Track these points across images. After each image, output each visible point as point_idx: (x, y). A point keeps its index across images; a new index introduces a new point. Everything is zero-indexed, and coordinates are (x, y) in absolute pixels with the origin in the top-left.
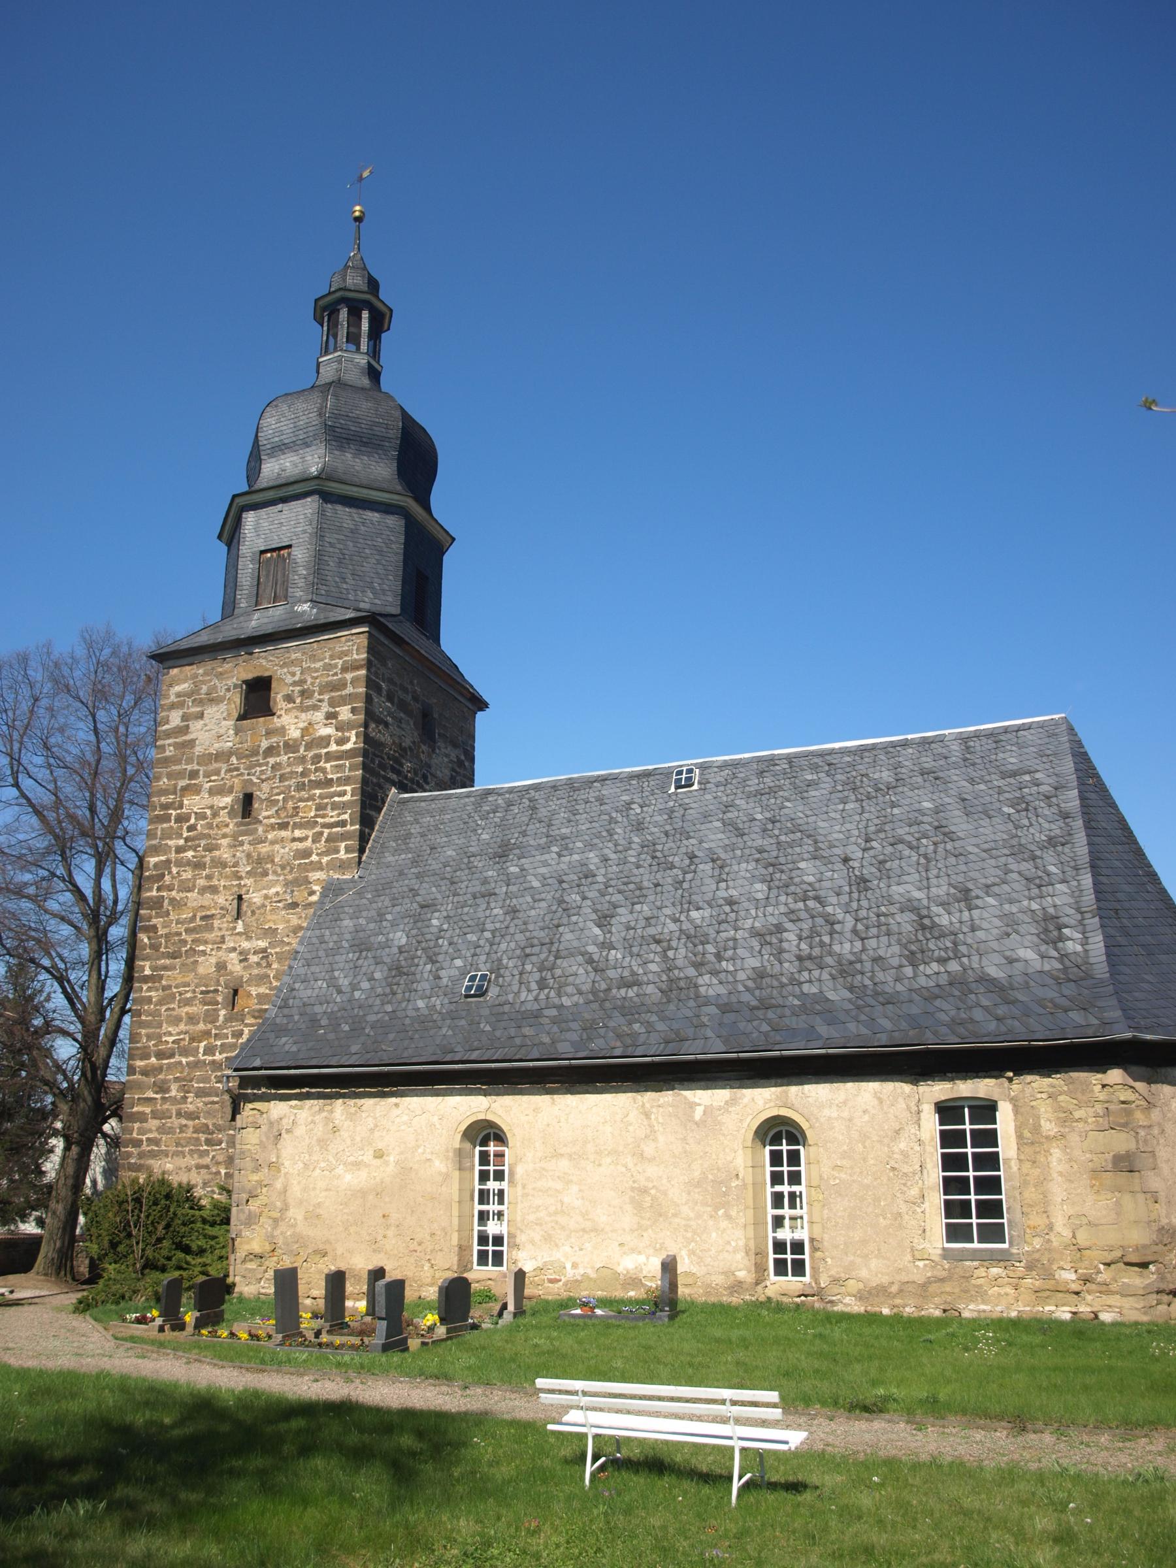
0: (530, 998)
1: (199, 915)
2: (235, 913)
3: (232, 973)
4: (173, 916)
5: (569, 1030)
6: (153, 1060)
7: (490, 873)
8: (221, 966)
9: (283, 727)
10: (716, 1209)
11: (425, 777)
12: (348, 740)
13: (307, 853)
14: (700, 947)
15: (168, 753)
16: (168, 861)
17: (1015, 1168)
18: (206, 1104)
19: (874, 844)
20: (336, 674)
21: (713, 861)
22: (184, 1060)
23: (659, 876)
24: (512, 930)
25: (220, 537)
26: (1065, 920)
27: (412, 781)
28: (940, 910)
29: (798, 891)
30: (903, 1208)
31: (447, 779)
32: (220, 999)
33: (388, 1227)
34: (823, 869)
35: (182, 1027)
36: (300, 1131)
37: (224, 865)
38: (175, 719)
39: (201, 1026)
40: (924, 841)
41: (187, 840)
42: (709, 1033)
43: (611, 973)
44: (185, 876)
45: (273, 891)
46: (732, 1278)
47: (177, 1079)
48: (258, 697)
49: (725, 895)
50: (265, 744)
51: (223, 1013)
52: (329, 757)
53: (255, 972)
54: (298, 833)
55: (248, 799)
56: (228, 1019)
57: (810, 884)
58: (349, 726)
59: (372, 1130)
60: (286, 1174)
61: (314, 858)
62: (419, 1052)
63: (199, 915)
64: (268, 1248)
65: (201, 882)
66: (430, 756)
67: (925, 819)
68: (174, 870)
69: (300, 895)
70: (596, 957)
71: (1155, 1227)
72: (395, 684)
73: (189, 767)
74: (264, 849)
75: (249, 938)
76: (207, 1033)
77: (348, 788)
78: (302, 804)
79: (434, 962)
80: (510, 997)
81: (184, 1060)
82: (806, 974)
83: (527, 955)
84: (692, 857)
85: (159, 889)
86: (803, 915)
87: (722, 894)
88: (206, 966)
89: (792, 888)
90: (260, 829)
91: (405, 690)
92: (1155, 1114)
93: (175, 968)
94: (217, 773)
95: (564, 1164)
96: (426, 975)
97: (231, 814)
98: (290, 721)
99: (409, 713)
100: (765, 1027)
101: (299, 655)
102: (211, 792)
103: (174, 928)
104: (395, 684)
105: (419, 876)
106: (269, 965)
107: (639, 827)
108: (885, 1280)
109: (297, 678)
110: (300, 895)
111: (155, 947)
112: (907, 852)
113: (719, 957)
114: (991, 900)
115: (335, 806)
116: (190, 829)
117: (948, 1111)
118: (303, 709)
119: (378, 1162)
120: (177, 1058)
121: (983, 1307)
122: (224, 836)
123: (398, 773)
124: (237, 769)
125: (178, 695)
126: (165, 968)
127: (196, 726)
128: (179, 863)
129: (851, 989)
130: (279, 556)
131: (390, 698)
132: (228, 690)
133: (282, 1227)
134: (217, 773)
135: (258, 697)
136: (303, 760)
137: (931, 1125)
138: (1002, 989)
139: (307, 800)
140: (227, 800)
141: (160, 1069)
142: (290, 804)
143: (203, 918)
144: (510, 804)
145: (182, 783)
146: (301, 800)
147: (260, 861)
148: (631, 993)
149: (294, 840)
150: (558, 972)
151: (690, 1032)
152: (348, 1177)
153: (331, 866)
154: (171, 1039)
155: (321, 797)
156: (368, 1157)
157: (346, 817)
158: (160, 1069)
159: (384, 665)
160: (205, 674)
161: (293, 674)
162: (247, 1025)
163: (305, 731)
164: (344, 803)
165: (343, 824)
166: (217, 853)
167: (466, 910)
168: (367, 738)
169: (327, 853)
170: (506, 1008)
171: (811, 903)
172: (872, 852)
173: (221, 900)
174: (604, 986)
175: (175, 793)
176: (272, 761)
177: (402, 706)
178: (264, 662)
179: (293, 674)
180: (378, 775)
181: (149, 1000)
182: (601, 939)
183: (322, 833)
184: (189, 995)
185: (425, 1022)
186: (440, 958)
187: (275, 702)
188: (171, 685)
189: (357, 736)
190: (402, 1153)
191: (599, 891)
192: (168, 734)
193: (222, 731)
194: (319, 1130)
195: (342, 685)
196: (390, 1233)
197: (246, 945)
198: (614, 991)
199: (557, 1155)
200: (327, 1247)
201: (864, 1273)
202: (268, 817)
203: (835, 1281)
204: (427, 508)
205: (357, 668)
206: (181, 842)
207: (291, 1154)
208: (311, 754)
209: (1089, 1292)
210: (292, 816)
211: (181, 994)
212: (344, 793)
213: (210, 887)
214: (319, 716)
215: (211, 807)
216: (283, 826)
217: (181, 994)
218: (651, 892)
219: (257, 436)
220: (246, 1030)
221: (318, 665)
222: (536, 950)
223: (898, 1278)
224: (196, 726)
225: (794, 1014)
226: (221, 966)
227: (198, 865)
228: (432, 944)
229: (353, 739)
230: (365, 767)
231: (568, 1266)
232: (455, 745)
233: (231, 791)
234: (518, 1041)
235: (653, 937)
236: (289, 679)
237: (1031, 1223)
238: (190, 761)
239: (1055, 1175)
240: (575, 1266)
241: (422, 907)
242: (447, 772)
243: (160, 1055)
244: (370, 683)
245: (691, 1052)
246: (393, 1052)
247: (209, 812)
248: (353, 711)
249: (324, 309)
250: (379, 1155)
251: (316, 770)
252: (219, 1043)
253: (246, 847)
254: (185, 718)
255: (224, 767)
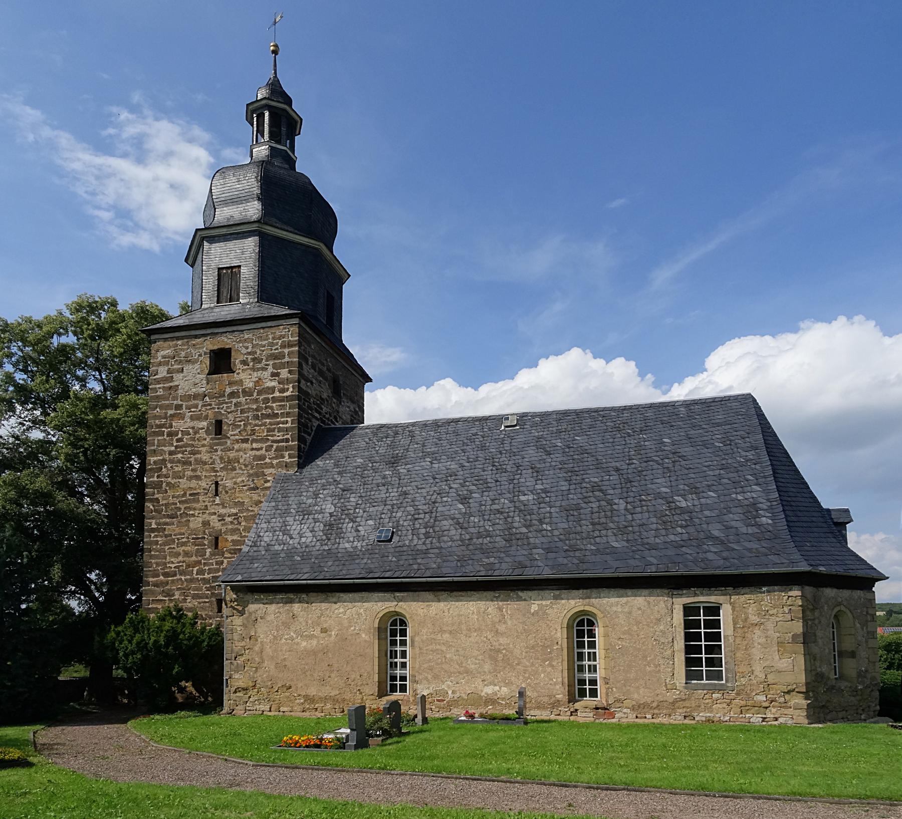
0: (420, 542)
1: (188, 493)
2: (214, 492)
3: (213, 527)
4: (170, 493)
5: (448, 561)
6: (162, 577)
7: (387, 473)
8: (206, 524)
9: (241, 380)
10: (544, 661)
11: (335, 418)
12: (288, 389)
13: (262, 458)
14: (528, 517)
15: (158, 393)
16: (164, 460)
17: (731, 640)
18: (200, 603)
19: (634, 461)
20: (277, 349)
21: (532, 468)
22: (183, 578)
23: (497, 476)
24: (404, 505)
25: (186, 260)
26: (760, 505)
27: (328, 419)
28: (680, 498)
29: (588, 486)
30: (661, 662)
31: (349, 421)
32: (206, 542)
33: (332, 671)
34: (603, 474)
35: (181, 558)
36: (271, 617)
37: (205, 463)
38: (162, 372)
39: (194, 558)
40: (667, 461)
41: (176, 447)
42: (540, 564)
43: (472, 530)
44: (176, 469)
45: (240, 479)
46: (554, 699)
47: (178, 589)
48: (221, 362)
49: (542, 487)
50: (228, 390)
51: (208, 550)
52: (274, 400)
53: (230, 527)
54: (255, 445)
55: (219, 425)
56: (212, 554)
57: (595, 482)
58: (288, 381)
59: (319, 617)
60: (261, 642)
61: (267, 460)
62: (354, 573)
63: (188, 493)
64: (251, 684)
65: (189, 473)
66: (338, 406)
67: (666, 448)
68: (169, 465)
69: (259, 482)
70: (461, 521)
71: (814, 673)
72: (316, 359)
73: (175, 402)
74: (232, 454)
75: (224, 507)
76: (199, 562)
77: (289, 419)
78: (257, 428)
79: (354, 522)
80: (407, 542)
81: (183, 578)
82: (597, 532)
83: (416, 519)
84: (518, 466)
85: (158, 477)
86: (592, 499)
87: (539, 487)
88: (196, 523)
89: (584, 485)
90: (229, 442)
91: (323, 364)
92: (817, 614)
93: (173, 524)
94: (196, 407)
95: (446, 636)
96: (349, 530)
97: (208, 432)
98: (246, 377)
99: (326, 379)
100: (576, 561)
101: (250, 336)
102: (192, 418)
103: (171, 500)
104: (316, 359)
105: (340, 473)
106: (239, 523)
107: (483, 448)
108: (649, 700)
109: (249, 350)
110: (259, 482)
111: (159, 512)
112: (656, 466)
113: (541, 522)
114: (711, 494)
115: (280, 430)
116: (178, 441)
117: (689, 610)
118: (254, 369)
119: (324, 635)
120: (178, 577)
121: (708, 715)
122: (203, 446)
123: (320, 413)
124: (210, 405)
125: (164, 357)
126: (167, 524)
127: (178, 377)
128: (171, 461)
129: (628, 541)
130: (232, 272)
131: (313, 367)
132: (200, 355)
133: (260, 672)
134: (196, 406)
135: (221, 362)
136: (256, 401)
137: (678, 617)
138: (723, 543)
139: (261, 425)
140: (204, 424)
141: (167, 583)
142: (249, 428)
143: (190, 495)
144: (396, 433)
145: (170, 412)
146: (256, 425)
147: (229, 461)
148: (485, 541)
149: (252, 449)
150: (437, 529)
151: (528, 563)
152: (304, 644)
153: (279, 465)
154: (173, 566)
155: (271, 424)
156: (317, 632)
157: (288, 436)
158: (167, 583)
159: (310, 346)
160: (183, 345)
161: (247, 348)
162: (226, 558)
163: (257, 383)
164: (287, 428)
165: (287, 440)
166: (199, 456)
167: (373, 493)
168: (300, 390)
169: (276, 458)
170: (405, 548)
171: (597, 493)
172: (633, 466)
173: (203, 484)
174: (468, 537)
175: (166, 418)
176: (234, 401)
177: (321, 373)
178: (225, 341)
179: (247, 348)
180: (308, 414)
181: (157, 543)
182: (464, 511)
183: (272, 446)
184: (184, 540)
185: (352, 556)
186: (358, 519)
187: (235, 364)
188: (158, 351)
189: (293, 387)
190: (340, 630)
191: (460, 484)
192: (158, 382)
193: (197, 381)
194: (283, 617)
195: (281, 356)
196: (333, 675)
197: (223, 511)
198: (475, 540)
199: (442, 631)
200: (292, 684)
201: (636, 696)
202: (234, 435)
203: (618, 701)
204: (332, 252)
205: (292, 346)
206: (173, 448)
207: (263, 632)
208: (262, 397)
209: (774, 707)
210: (251, 435)
211: (178, 539)
212: (287, 422)
213: (196, 476)
214: (266, 374)
215: (193, 428)
216: (245, 441)
217: (178, 539)
218: (493, 485)
219: (211, 189)
220: (225, 561)
221: (264, 343)
222: (422, 516)
223: (657, 698)
224: (178, 377)
225: (592, 554)
226: (206, 524)
227: (187, 463)
228: (352, 512)
229: (291, 389)
230: (300, 407)
231: (450, 692)
232: (353, 402)
233: (206, 418)
234: (415, 567)
235: (498, 510)
236: (244, 351)
237: (740, 670)
238: (175, 398)
239: (756, 644)
240: (453, 692)
241: (344, 491)
242: (349, 417)
243: (166, 575)
244: (301, 355)
245: (530, 574)
246: (331, 572)
247: (191, 431)
248: (290, 372)
249: (253, 112)
250: (324, 631)
251: (266, 408)
252: (207, 568)
253: (219, 453)
254: (169, 372)
255: (200, 403)
